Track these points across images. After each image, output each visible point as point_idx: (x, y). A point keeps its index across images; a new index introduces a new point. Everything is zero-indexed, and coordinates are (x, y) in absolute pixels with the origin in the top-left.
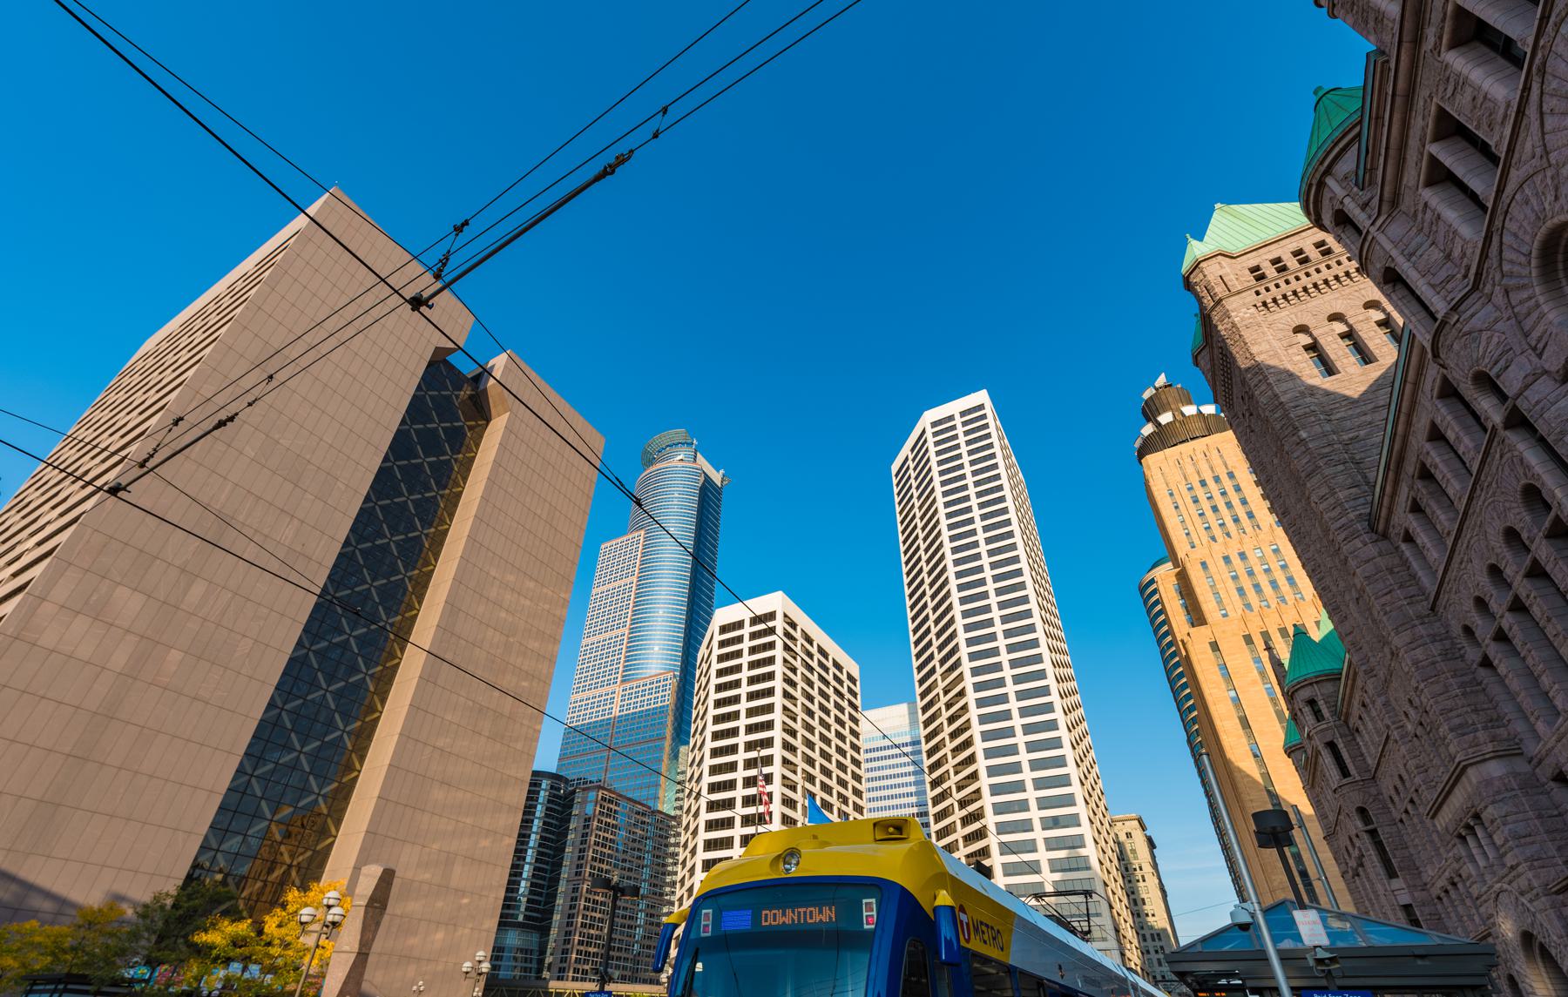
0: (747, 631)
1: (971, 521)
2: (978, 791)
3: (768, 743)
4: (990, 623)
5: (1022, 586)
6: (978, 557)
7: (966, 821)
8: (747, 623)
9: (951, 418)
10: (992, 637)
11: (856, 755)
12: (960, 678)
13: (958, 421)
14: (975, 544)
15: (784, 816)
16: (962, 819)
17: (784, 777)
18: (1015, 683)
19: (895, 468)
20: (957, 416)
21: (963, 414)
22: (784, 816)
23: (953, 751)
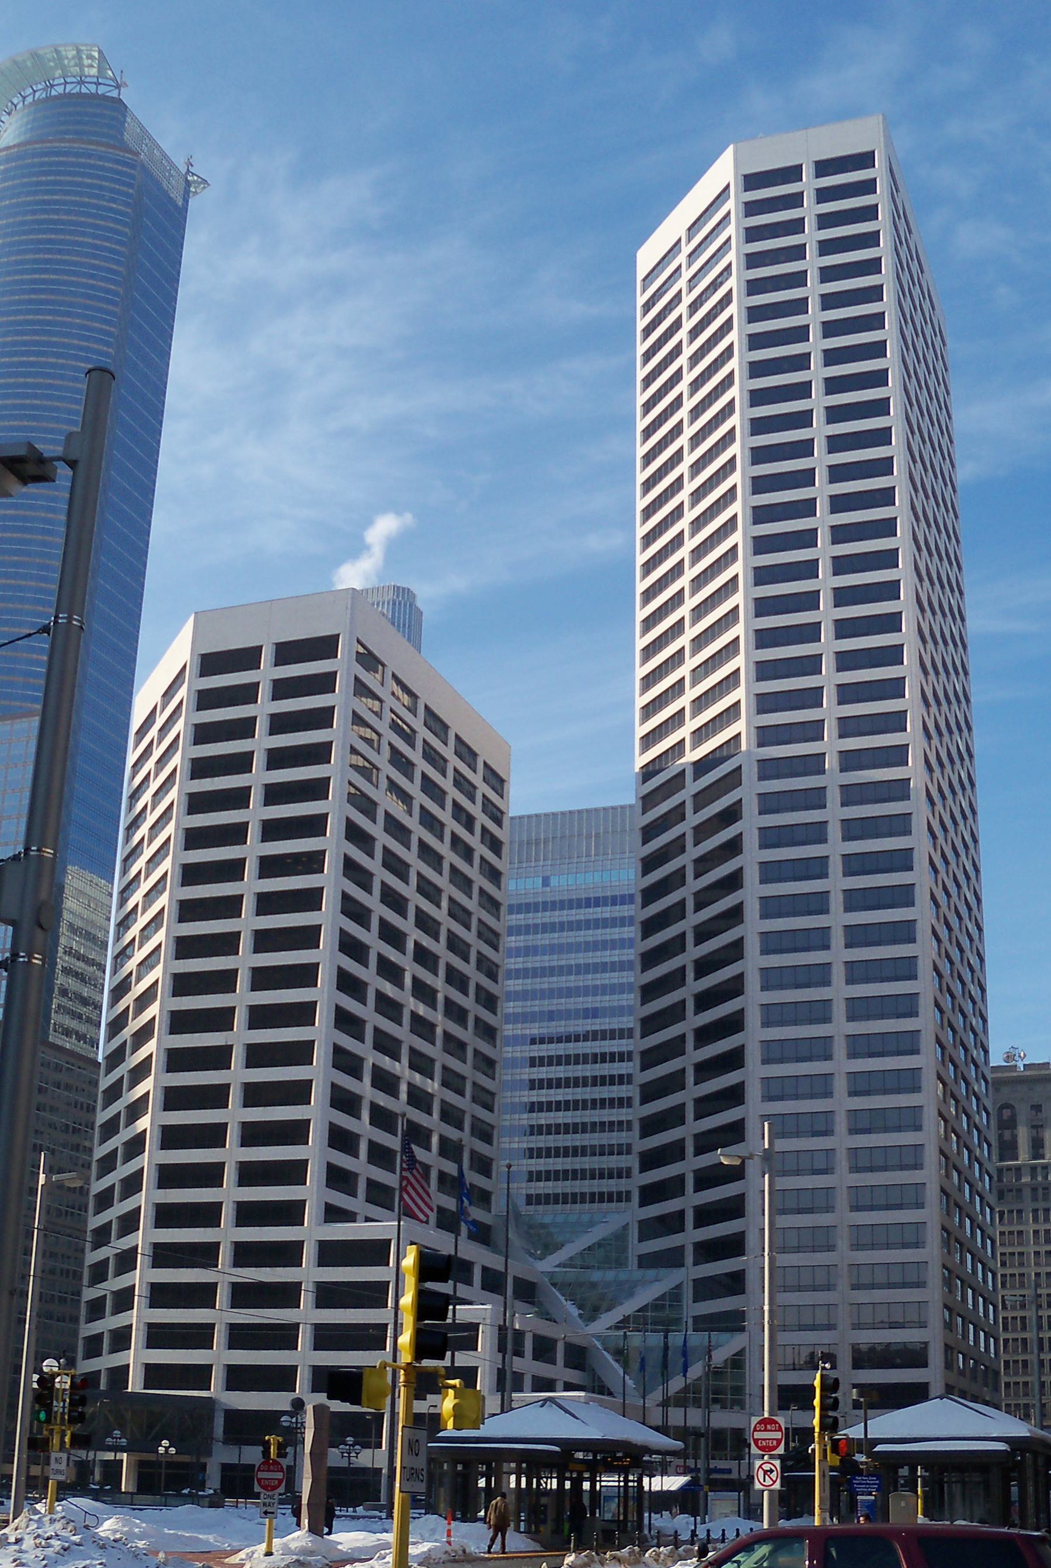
0: (266, 673)
1: (808, 539)
2: (740, 977)
3: (315, 826)
4: (808, 539)
5: (886, 497)
6: (799, 306)
7: (706, 1070)
8: (267, 657)
9: (793, 173)
10: (811, 665)
11: (490, 921)
12: (735, 915)
13: (808, 184)
14: (798, 279)
15: (338, 1050)
16: (698, 1101)
17: (345, 897)
18: (850, 981)
19: (647, 257)
20: (807, 173)
21: (823, 168)
22: (338, 1050)
23: (697, 829)
